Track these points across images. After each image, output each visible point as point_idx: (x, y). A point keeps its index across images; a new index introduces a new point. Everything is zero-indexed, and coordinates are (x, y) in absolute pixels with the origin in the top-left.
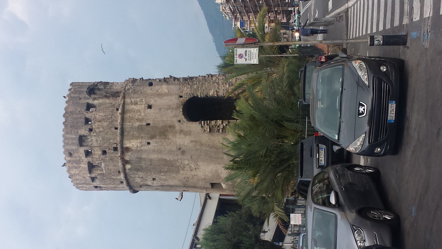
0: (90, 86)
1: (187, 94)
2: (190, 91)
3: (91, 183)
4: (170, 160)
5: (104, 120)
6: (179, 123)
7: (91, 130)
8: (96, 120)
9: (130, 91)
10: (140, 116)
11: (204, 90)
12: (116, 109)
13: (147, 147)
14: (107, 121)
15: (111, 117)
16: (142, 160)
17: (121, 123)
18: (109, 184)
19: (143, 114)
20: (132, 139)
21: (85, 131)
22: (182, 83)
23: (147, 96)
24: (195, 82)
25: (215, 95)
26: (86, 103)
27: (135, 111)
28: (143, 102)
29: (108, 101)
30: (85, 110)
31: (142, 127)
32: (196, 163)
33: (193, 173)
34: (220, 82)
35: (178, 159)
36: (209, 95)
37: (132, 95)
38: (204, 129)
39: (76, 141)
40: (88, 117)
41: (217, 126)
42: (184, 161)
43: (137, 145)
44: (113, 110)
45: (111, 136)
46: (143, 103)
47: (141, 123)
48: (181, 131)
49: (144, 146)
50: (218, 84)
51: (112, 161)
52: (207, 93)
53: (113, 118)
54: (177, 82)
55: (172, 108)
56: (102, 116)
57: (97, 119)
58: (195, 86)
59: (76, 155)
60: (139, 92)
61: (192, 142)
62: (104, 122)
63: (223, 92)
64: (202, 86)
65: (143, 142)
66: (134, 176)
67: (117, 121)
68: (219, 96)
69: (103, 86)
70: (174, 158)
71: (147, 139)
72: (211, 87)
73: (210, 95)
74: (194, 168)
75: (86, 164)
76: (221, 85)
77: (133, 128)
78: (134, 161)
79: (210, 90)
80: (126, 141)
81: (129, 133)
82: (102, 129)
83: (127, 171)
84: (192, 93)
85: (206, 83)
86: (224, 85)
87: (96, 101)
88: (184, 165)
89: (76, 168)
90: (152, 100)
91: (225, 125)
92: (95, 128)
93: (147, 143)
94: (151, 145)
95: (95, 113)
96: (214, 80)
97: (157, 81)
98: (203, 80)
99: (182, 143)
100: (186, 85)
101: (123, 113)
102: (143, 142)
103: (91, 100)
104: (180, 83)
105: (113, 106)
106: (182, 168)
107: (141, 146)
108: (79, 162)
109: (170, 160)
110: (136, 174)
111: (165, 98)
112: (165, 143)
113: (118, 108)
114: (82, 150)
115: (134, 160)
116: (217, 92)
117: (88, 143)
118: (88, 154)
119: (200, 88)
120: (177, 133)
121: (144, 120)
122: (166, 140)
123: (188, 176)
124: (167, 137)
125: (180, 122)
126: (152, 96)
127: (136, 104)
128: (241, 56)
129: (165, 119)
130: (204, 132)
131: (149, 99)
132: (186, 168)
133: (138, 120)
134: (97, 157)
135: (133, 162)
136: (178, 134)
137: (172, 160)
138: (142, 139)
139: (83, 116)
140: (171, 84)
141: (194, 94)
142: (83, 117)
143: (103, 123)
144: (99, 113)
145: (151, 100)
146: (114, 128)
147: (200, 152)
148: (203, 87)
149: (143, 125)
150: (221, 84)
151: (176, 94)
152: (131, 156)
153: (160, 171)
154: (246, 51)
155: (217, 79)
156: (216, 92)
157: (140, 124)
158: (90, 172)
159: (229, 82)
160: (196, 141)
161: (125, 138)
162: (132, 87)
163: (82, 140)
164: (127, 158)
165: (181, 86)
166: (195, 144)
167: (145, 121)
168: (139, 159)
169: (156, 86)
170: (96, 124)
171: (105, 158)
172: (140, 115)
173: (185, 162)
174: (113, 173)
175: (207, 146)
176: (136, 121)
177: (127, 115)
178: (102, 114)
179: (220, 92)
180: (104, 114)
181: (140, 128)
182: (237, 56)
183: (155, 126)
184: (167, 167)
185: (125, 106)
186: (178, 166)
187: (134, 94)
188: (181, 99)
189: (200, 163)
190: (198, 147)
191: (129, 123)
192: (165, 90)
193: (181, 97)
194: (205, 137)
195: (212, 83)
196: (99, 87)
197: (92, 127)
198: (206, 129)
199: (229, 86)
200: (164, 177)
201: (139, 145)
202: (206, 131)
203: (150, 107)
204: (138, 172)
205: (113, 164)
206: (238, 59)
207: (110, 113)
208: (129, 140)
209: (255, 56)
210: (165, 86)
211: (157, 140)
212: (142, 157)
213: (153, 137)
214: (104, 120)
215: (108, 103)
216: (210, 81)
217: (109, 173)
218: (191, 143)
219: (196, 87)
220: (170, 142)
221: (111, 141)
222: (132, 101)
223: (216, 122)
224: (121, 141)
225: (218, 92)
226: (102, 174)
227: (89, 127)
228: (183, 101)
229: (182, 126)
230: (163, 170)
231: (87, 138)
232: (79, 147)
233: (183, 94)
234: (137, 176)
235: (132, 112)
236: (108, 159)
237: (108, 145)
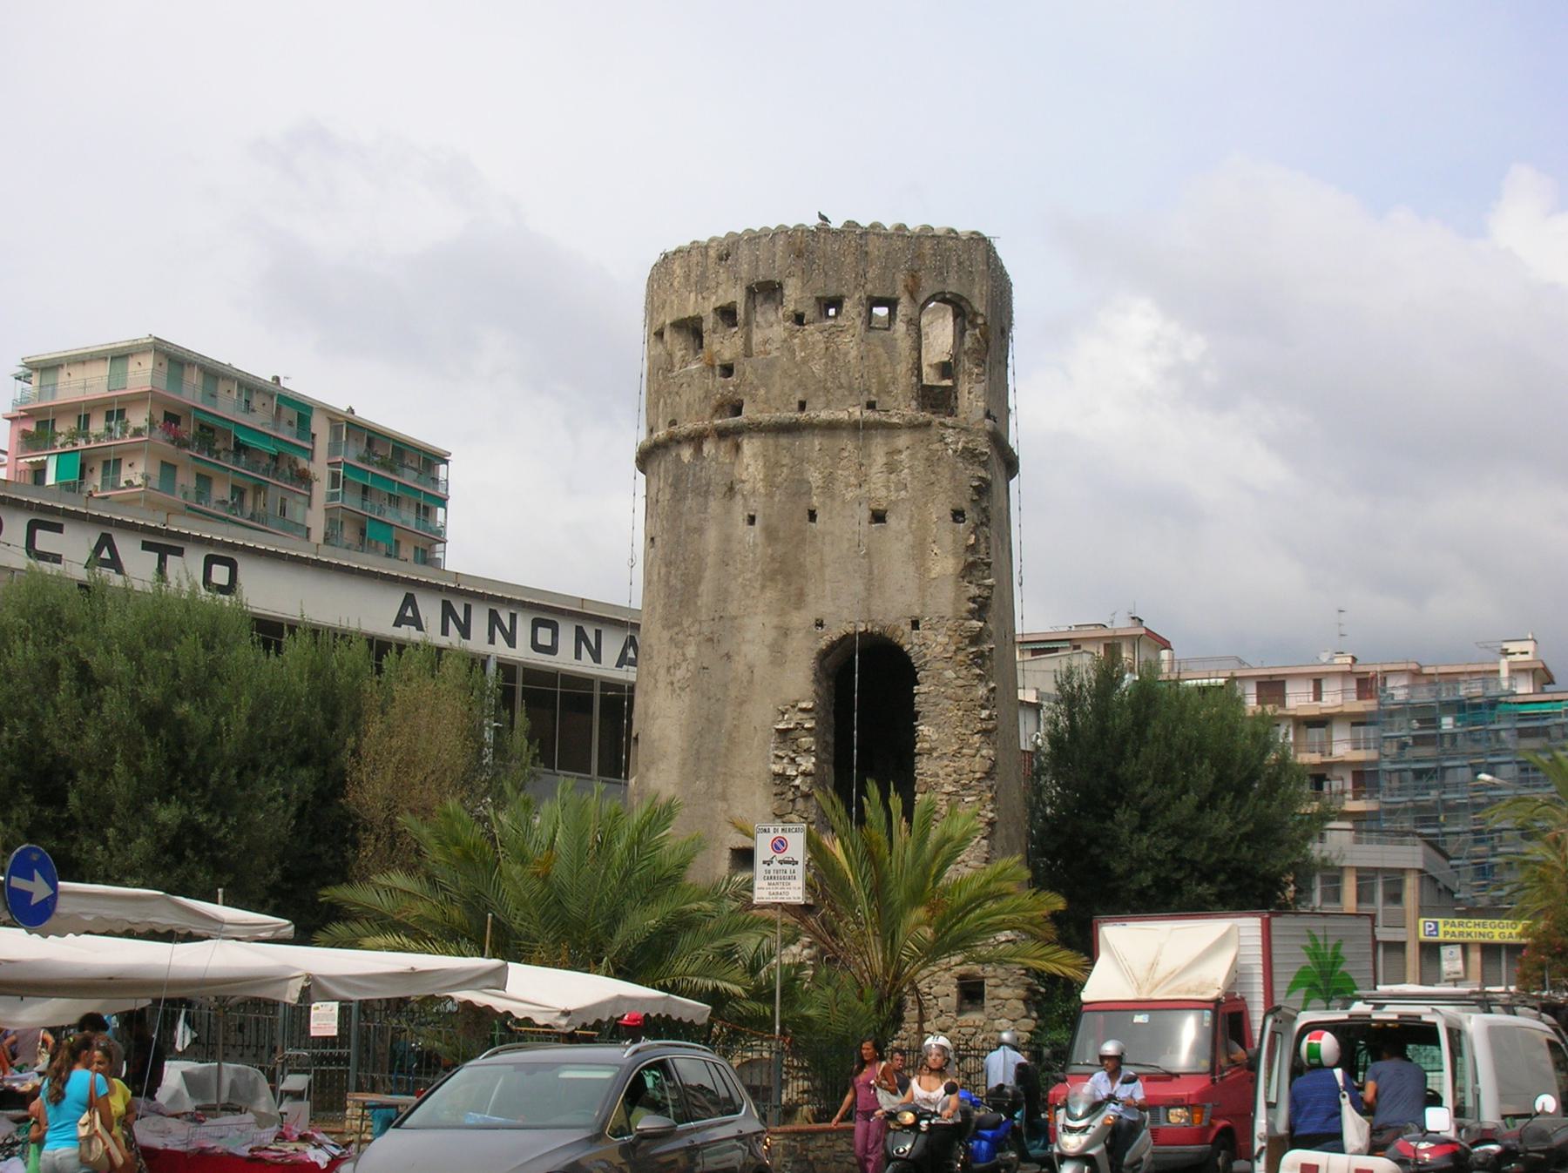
0: (969, 303)
3: (653, 331)
4: (698, 596)
5: (833, 362)
6: (813, 622)
7: (799, 319)
8: (833, 336)
9: (936, 446)
11: (938, 705)
12: (873, 398)
13: (740, 515)
15: (841, 387)
16: (701, 499)
19: (849, 496)
21: (796, 301)
23: (917, 507)
24: (965, 672)
25: (918, 746)
26: (895, 296)
29: (904, 371)
30: (869, 293)
31: (805, 493)
33: (662, 674)
34: (964, 762)
36: (922, 724)
37: (923, 453)
38: (787, 710)
41: (793, 755)
44: (870, 392)
45: (775, 391)
47: (819, 490)
48: (784, 632)
49: (745, 506)
50: (957, 754)
51: (702, 396)
53: (839, 393)
54: (963, 609)
55: (870, 595)
56: (846, 354)
57: (838, 336)
59: (723, 276)
60: (932, 476)
62: (826, 363)
63: (929, 773)
64: (951, 699)
67: (827, 406)
68: (917, 759)
69: (970, 345)
70: (704, 610)
71: (764, 515)
73: (920, 728)
74: (675, 680)
76: (952, 764)
82: (802, 357)
85: (960, 713)
86: (954, 775)
87: (905, 328)
89: (687, 276)
90: (904, 524)
91: (798, 782)
92: (806, 332)
93: (752, 513)
95: (858, 329)
97: (968, 539)
98: (972, 700)
99: (749, 636)
103: (909, 312)
104: (961, 618)
105: (884, 388)
108: (702, 286)
109: (698, 596)
111: (911, 570)
112: (749, 575)
113: (877, 406)
114: (735, 295)
115: (703, 474)
116: (930, 751)
117: (763, 313)
118: (727, 314)
120: (780, 615)
121: (828, 501)
122: (759, 578)
123: (655, 659)
124: (768, 583)
125: (817, 625)
126: (919, 521)
127: (891, 468)
128: (779, 845)
129: (828, 572)
131: (908, 512)
133: (829, 479)
134: (714, 347)
136: (775, 621)
137: (699, 603)
139: (848, 290)
140: (958, 588)
142: (844, 290)
143: (820, 359)
145: (902, 519)
146: (803, 399)
148: (947, 703)
149: (811, 498)
150: (956, 765)
154: (797, 863)
155: (973, 752)
156: (929, 750)
159: (961, 793)
160: (751, 682)
163: (766, 291)
164: (708, 448)
165: (950, 622)
166: (742, 682)
167: (824, 504)
170: (817, 336)
172: (848, 485)
173: (691, 648)
176: (827, 471)
177: (848, 444)
178: (853, 353)
181: (800, 488)
182: (780, 834)
183: (804, 540)
184: (679, 586)
185: (884, 432)
188: (907, 624)
189: (686, 698)
190: (733, 693)
192: (938, 569)
193: (915, 625)
194: (762, 716)
196: (968, 332)
197: (808, 323)
198: (786, 716)
199: (948, 794)
200: (655, 578)
201: (748, 486)
202: (780, 718)
203: (879, 517)
204: (671, 486)
206: (772, 836)
209: (779, 891)
211: (760, 548)
212: (711, 498)
213: (771, 534)
214: (833, 362)
215: (894, 371)
216: (966, 726)
218: (746, 668)
219: (948, 676)
220: (753, 593)
222: (900, 452)
223: (808, 751)
226: (673, 365)
227: (810, 314)
231: (777, 309)
232: (744, 284)
234: (662, 485)
237: (748, 381)
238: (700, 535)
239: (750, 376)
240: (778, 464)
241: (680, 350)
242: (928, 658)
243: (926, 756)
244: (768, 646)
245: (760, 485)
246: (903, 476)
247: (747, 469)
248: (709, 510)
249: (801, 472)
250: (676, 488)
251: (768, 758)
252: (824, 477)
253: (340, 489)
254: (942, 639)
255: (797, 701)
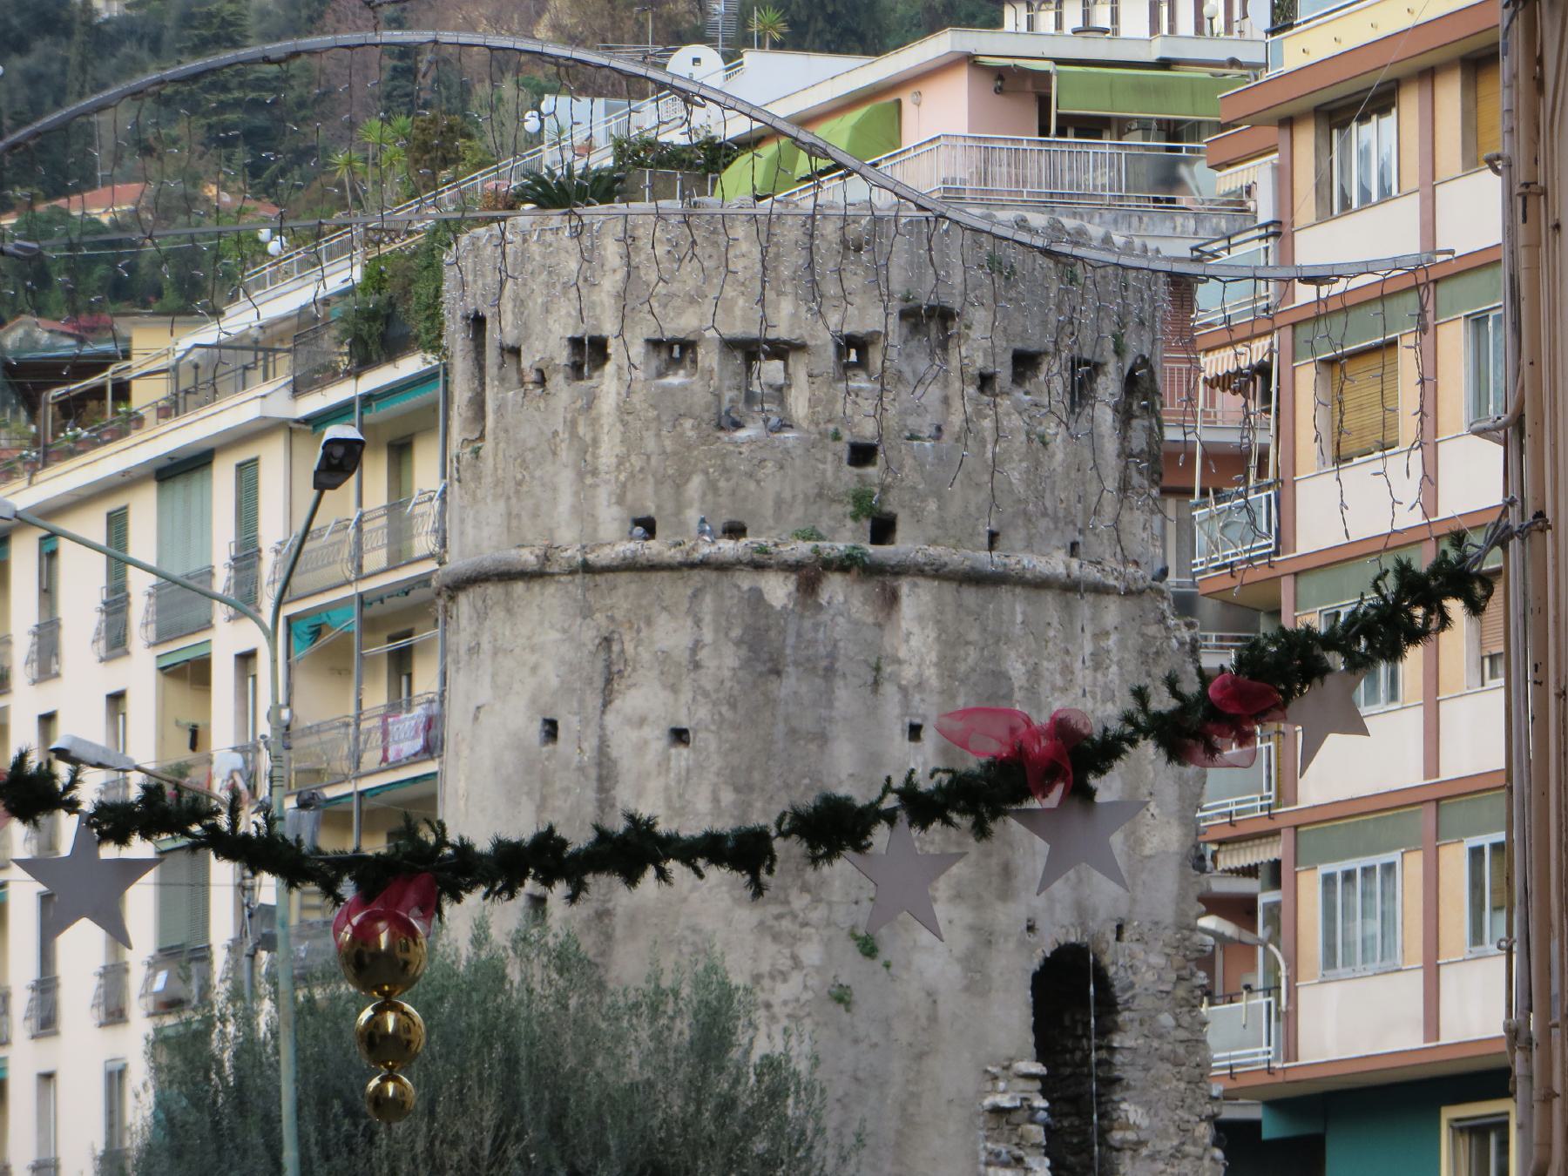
1: (1131, 967)
2: (1146, 989)
7: (985, 381)
9: (1153, 630)
10: (1048, 686)
14: (1028, 486)
15: (1044, 514)
17: (1028, 575)
18: (631, 443)
20: (944, 637)
22: (1187, 943)
26: (1101, 360)
27: (1068, 659)
28: (1104, 702)
32: (809, 1015)
35: (830, 904)
36: (1124, 1100)
39: (925, 296)
40: (1044, 367)
42: (816, 938)
43: (905, 661)
45: (955, 509)
46: (1098, 705)
48: (985, 937)
51: (813, 492)
52: (1135, 1088)
53: (1044, 524)
58: (1166, 1019)
59: (854, 282)
61: (931, 995)
62: (1028, 471)
64: (1168, 1060)
65: (923, 700)
66: (708, 618)
67: (1029, 547)
70: (837, 883)
72: (1161, 1113)
73: (1124, 1106)
75: (798, 331)
77: (997, 642)
78: (817, 631)
79: (1148, 1106)
80: (928, 598)
81: (972, 618)
83: (746, 580)
84: (1133, 997)
88: (795, 939)
93: (917, 721)
94: (908, 745)
96: (1197, 1134)
98: (1198, 1065)
100: (1176, 965)
101: (1070, 587)
102: (923, 700)
106: (776, 923)
107: (904, 682)
110: (727, 634)
114: (867, 317)
115: (821, 635)
119: (1157, 1049)
130: (986, 1071)
132: (770, 948)
133: (1034, 673)
135: (808, 624)
138: (942, 692)
141: (1129, 1009)
143: (1020, 461)
144: (1064, 441)
146: (994, 527)
147: (874, 1040)
148: (1165, 1069)
151: (1134, 901)
152: (842, 615)
153: (750, 788)
155: (1200, 1151)
157: (1016, 685)
158: (730, 345)
160: (933, 1019)
161: (949, 589)
162: (1174, 640)
164: (835, 588)
166: (917, 1018)
168: (824, 663)
169: (1176, 787)
171: (830, 457)
174: (734, 493)
175: (911, 1088)
176: (1031, 661)
177: (1050, 604)
179: (1138, 1164)
180: (1060, 469)
186: (787, 902)
187: (1141, 652)
190: (903, 1033)
191: (1019, 618)
195: (1181, 1119)
196: (1135, 423)
202: (989, 1086)
204: (739, 643)
205: (794, 497)
207: (1064, 505)
208: (939, 617)
210: (1175, 838)
212: (839, 683)
217: (728, 463)
221: (932, 505)
223: (1036, 1146)
224: (937, 571)
225: (1135, 1151)
228: (1104, 946)
229: (1011, 945)
230: (759, 805)
233: (1131, 945)
234: (708, 636)
235: (1066, 639)
236: (824, 472)
237: (908, 483)
238: (821, 747)
239: (910, 475)
240: (961, 641)
241: (730, 389)
242: (1137, 990)
243: (1129, 1153)
244: (959, 960)
245: (931, 673)
246: (1110, 677)
247: (907, 641)
248: (837, 704)
249: (995, 658)
250: (751, 648)
251: (976, 1155)
252: (1028, 672)
253: (438, 631)
254: (1157, 960)
255: (1011, 1059)
